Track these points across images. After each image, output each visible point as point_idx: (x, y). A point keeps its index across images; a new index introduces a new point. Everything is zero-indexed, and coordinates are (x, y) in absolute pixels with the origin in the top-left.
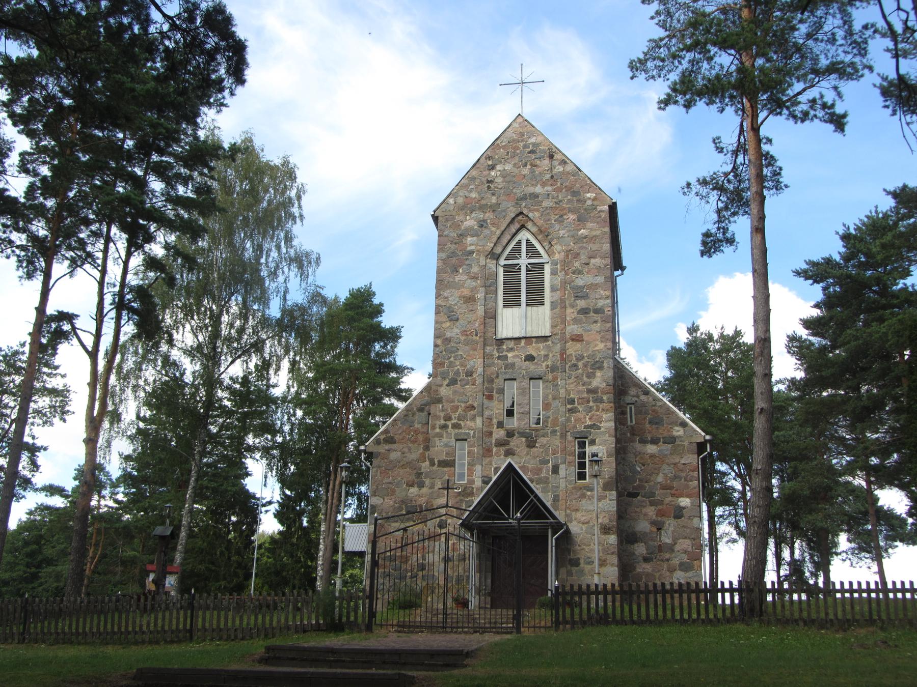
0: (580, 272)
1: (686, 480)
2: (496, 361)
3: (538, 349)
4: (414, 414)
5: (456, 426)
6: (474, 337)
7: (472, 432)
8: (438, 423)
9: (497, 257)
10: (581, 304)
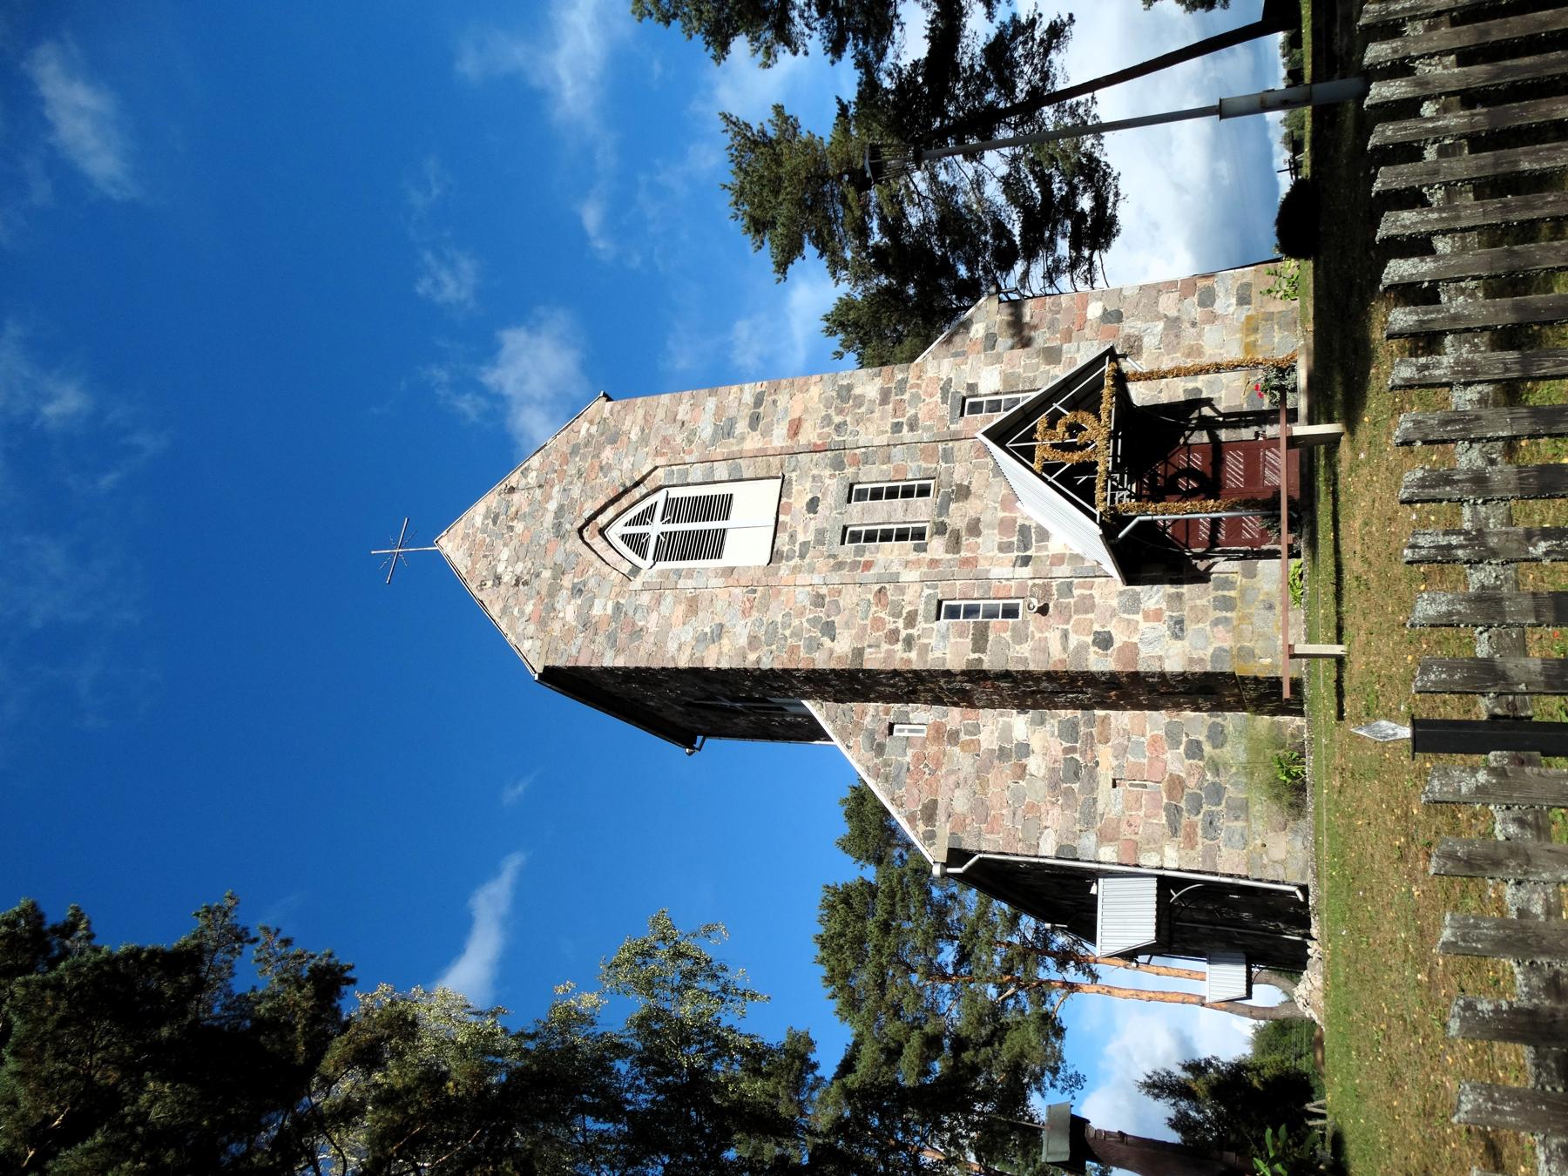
0: (693, 432)
1: (1058, 312)
2: (807, 560)
3: (800, 492)
4: (887, 764)
5: (911, 620)
6: (758, 595)
7: (927, 591)
8: (900, 654)
9: (636, 570)
10: (742, 426)
